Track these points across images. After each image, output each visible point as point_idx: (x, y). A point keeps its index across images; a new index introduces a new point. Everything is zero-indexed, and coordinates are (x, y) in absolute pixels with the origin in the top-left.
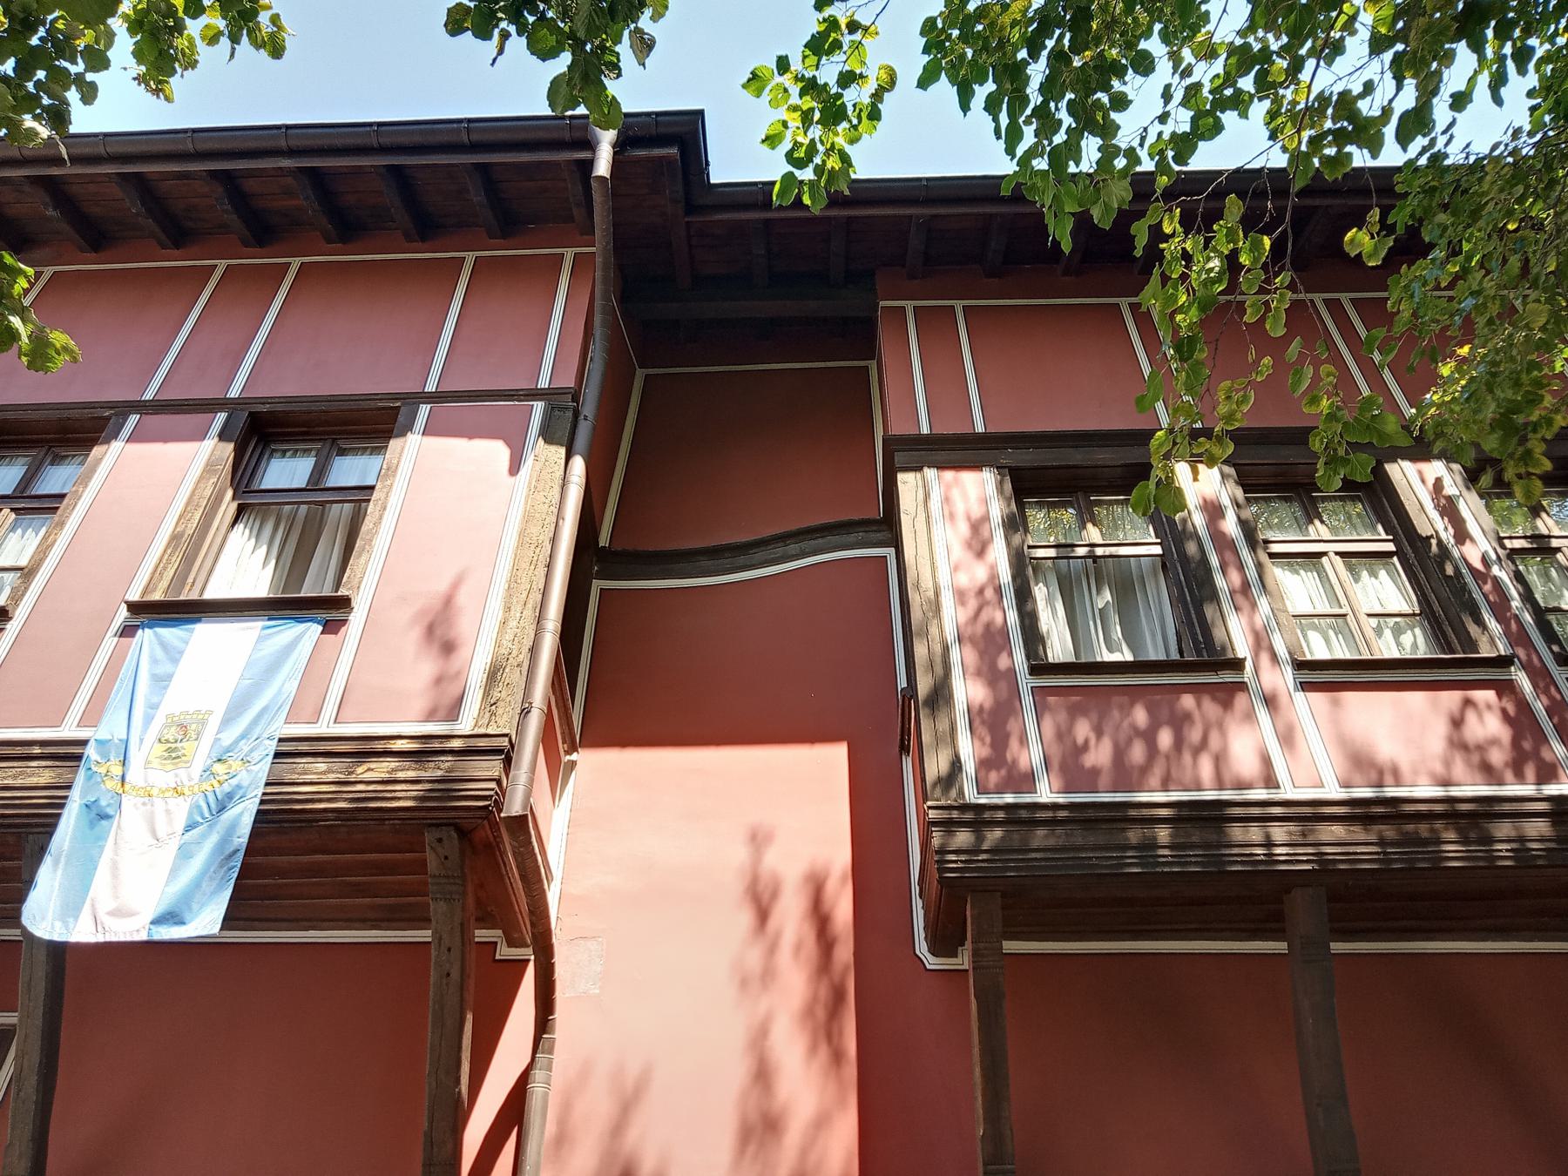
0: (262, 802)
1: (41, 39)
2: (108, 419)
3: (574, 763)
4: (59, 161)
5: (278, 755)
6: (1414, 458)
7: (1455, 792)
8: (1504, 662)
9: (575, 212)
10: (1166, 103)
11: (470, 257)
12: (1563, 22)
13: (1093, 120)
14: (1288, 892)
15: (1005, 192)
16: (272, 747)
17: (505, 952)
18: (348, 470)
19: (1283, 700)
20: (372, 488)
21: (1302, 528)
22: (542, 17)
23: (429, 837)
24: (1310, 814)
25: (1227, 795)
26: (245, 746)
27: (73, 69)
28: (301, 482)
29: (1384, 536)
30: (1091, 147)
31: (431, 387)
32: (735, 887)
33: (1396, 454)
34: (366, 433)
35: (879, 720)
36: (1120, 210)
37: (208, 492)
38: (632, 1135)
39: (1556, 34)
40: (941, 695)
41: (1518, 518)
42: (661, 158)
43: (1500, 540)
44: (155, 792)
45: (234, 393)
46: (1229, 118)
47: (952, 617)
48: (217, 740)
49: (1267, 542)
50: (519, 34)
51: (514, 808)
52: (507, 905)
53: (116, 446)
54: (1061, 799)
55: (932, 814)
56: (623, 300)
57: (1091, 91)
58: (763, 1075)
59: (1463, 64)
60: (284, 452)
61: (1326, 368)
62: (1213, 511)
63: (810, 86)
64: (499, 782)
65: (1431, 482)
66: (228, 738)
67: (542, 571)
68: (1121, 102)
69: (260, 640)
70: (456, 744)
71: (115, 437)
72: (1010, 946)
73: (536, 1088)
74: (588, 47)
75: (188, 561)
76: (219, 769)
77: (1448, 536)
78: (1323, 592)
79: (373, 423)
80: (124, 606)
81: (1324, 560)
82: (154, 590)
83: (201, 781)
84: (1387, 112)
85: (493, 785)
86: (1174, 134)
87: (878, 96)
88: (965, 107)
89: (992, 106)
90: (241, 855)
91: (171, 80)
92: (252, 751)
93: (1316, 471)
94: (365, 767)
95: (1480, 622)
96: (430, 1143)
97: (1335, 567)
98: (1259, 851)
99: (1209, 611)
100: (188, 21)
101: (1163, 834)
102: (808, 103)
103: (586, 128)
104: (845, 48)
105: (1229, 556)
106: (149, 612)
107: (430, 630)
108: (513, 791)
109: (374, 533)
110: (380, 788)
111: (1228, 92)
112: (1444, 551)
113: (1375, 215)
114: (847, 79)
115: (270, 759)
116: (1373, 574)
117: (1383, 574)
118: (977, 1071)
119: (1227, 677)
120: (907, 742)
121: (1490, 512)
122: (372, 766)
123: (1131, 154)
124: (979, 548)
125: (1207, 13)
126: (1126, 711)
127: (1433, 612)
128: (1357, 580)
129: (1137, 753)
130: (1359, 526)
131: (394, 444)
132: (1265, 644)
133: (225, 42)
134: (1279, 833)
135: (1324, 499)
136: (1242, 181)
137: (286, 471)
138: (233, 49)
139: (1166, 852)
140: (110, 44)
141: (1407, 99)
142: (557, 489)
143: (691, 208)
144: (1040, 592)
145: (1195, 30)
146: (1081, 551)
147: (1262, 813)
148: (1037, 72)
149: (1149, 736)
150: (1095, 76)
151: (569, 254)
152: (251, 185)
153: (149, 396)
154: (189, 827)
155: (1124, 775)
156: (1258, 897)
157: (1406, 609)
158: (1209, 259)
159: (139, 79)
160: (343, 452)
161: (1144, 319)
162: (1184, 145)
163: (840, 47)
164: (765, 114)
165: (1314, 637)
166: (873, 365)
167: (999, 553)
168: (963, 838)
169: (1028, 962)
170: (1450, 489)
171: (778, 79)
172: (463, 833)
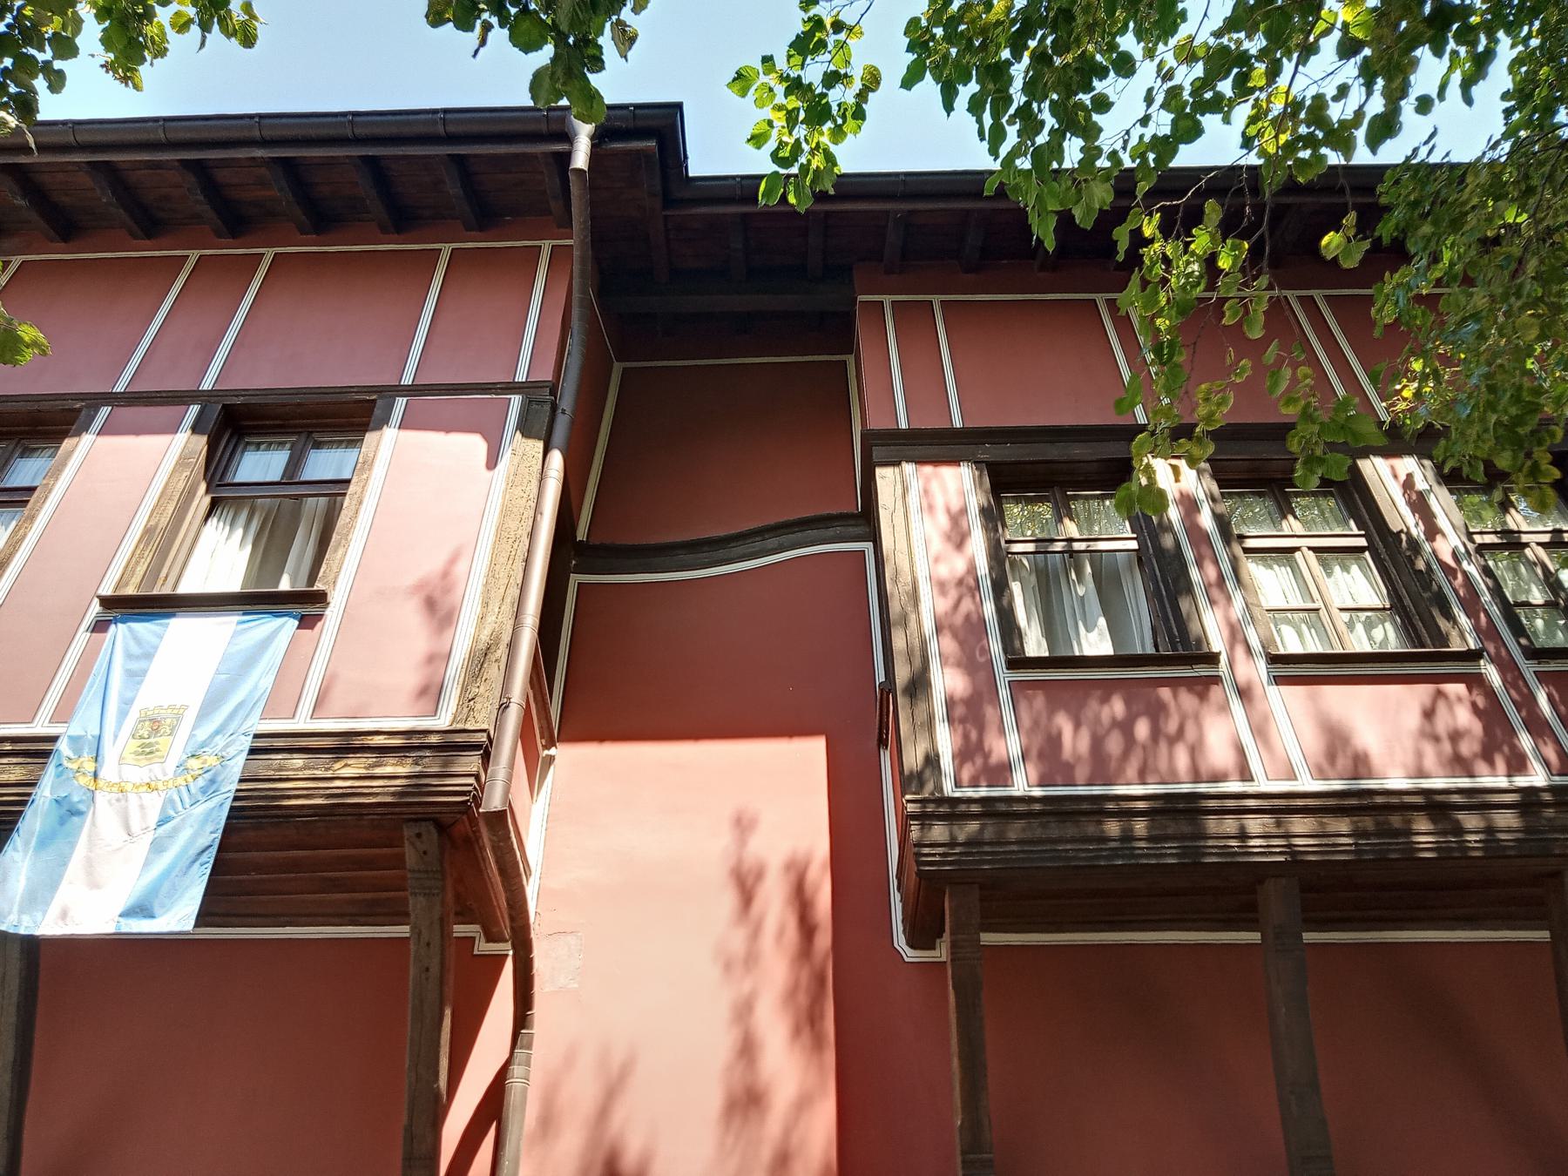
0: (236, 799)
1: (8, 26)
2: (79, 410)
3: (551, 759)
4: (26, 149)
5: (253, 751)
6: (1387, 453)
8: (1473, 656)
9: (553, 204)
10: (1149, 106)
11: (446, 249)
12: (1537, 24)
13: (1076, 122)
14: (1261, 882)
15: (989, 189)
16: (247, 743)
17: (483, 947)
18: (323, 463)
19: (1258, 691)
20: (348, 482)
21: (1275, 524)
22: (525, 10)
23: (408, 832)
24: (1282, 806)
25: (1203, 788)
26: (220, 741)
27: (41, 57)
28: (275, 475)
29: (1356, 532)
30: (1073, 150)
31: (407, 380)
33: (1366, 453)
34: (335, 426)
35: (859, 715)
36: (1101, 210)
37: (181, 485)
39: (1529, 36)
40: (919, 685)
41: (1488, 514)
42: (638, 151)
43: (1470, 535)
44: (129, 787)
45: (207, 385)
46: (1210, 121)
47: (931, 606)
48: (191, 736)
49: (1242, 537)
50: (502, 26)
51: (493, 802)
52: (485, 898)
53: (87, 439)
54: (1037, 792)
55: (911, 808)
56: (602, 292)
57: (1071, 88)
58: (747, 1049)
59: (1429, 70)
60: (270, 444)
61: (1304, 370)
62: (1190, 505)
63: (795, 86)
64: (477, 777)
65: (1403, 478)
66: (203, 734)
67: (519, 566)
68: (1103, 104)
69: (236, 634)
70: (434, 739)
71: (86, 429)
72: (988, 938)
73: (515, 1083)
74: (571, 40)
75: (162, 553)
76: (194, 764)
77: (1418, 532)
78: (1296, 587)
79: (349, 416)
80: (96, 601)
81: (1298, 555)
82: (127, 584)
83: (176, 775)
84: (1359, 113)
85: (471, 780)
86: (1154, 136)
87: (862, 96)
88: (949, 107)
89: (975, 107)
90: (214, 850)
91: (140, 68)
92: (227, 746)
93: (1293, 471)
94: (342, 763)
95: (1450, 617)
96: (410, 1137)
97: (1308, 562)
98: (1233, 843)
99: (1185, 604)
100: (158, 9)
101: (1140, 827)
102: (793, 102)
103: (563, 120)
104: (830, 47)
105: (1205, 550)
106: (121, 607)
108: (492, 788)
109: (350, 527)
110: (357, 783)
111: (1209, 95)
112: (1415, 546)
113: (1350, 219)
114: (832, 79)
115: (244, 755)
116: (1345, 569)
117: (1355, 568)
118: (955, 1062)
119: (1202, 671)
120: (885, 735)
121: (1461, 508)
122: (350, 762)
123: (1113, 155)
124: (958, 539)
125: (1184, 12)
126: (1105, 700)
127: (1404, 607)
128: (1329, 575)
129: (1114, 744)
130: (1331, 520)
131: (370, 437)
132: (1240, 637)
133: (195, 30)
134: (1254, 824)
135: (1297, 495)
136: (1224, 182)
137: (260, 464)
138: (204, 37)
139: (1142, 844)
140: (77, 29)
141: (1376, 105)
142: (535, 483)
143: (668, 201)
144: (1016, 587)
145: (1173, 30)
146: (1059, 546)
147: (1237, 806)
148: (1019, 71)
149: (1126, 727)
150: (1076, 78)
151: (546, 245)
152: (222, 175)
153: (120, 387)
154: (160, 823)
156: (1230, 889)
157: (1377, 603)
158: (1188, 263)
159: (107, 67)
160: (318, 445)
161: (1124, 324)
162: (1165, 146)
163: (825, 46)
164: (750, 113)
165: (1287, 630)
166: (851, 359)
167: (977, 544)
168: (939, 832)
169: (1007, 958)
170: (1421, 485)
171: (763, 79)
172: (442, 828)
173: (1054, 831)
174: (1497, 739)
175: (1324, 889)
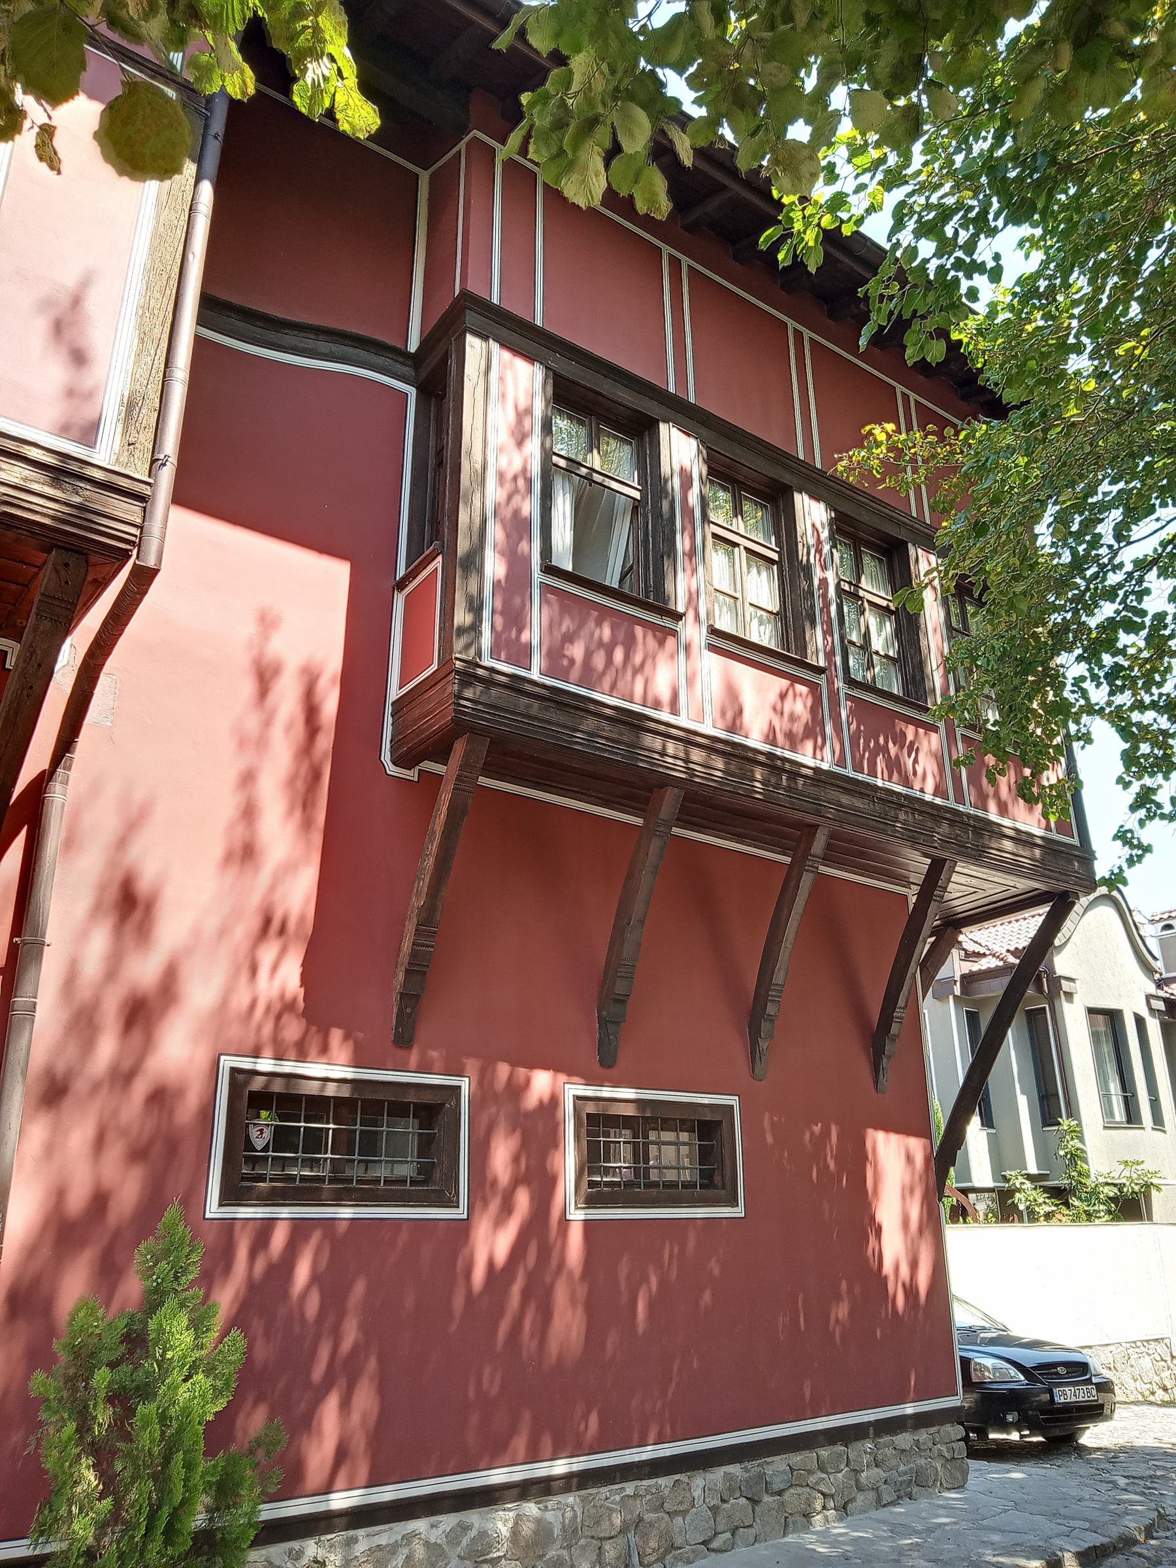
7: (778, 752)
8: (820, 671)
19: (695, 650)
24: (689, 739)
32: (243, 660)
38: (135, 852)
47: (494, 493)
72: (483, 781)
81: (736, 549)
97: (740, 554)
105: (689, 527)
107: (58, 328)
117: (764, 574)
119: (667, 622)
124: (520, 439)
129: (599, 661)
134: (671, 748)
146: (584, 471)
147: (665, 732)
155: (589, 677)
156: (635, 785)
167: (533, 446)
173: (553, 715)
174: (813, 730)
175: (705, 806)
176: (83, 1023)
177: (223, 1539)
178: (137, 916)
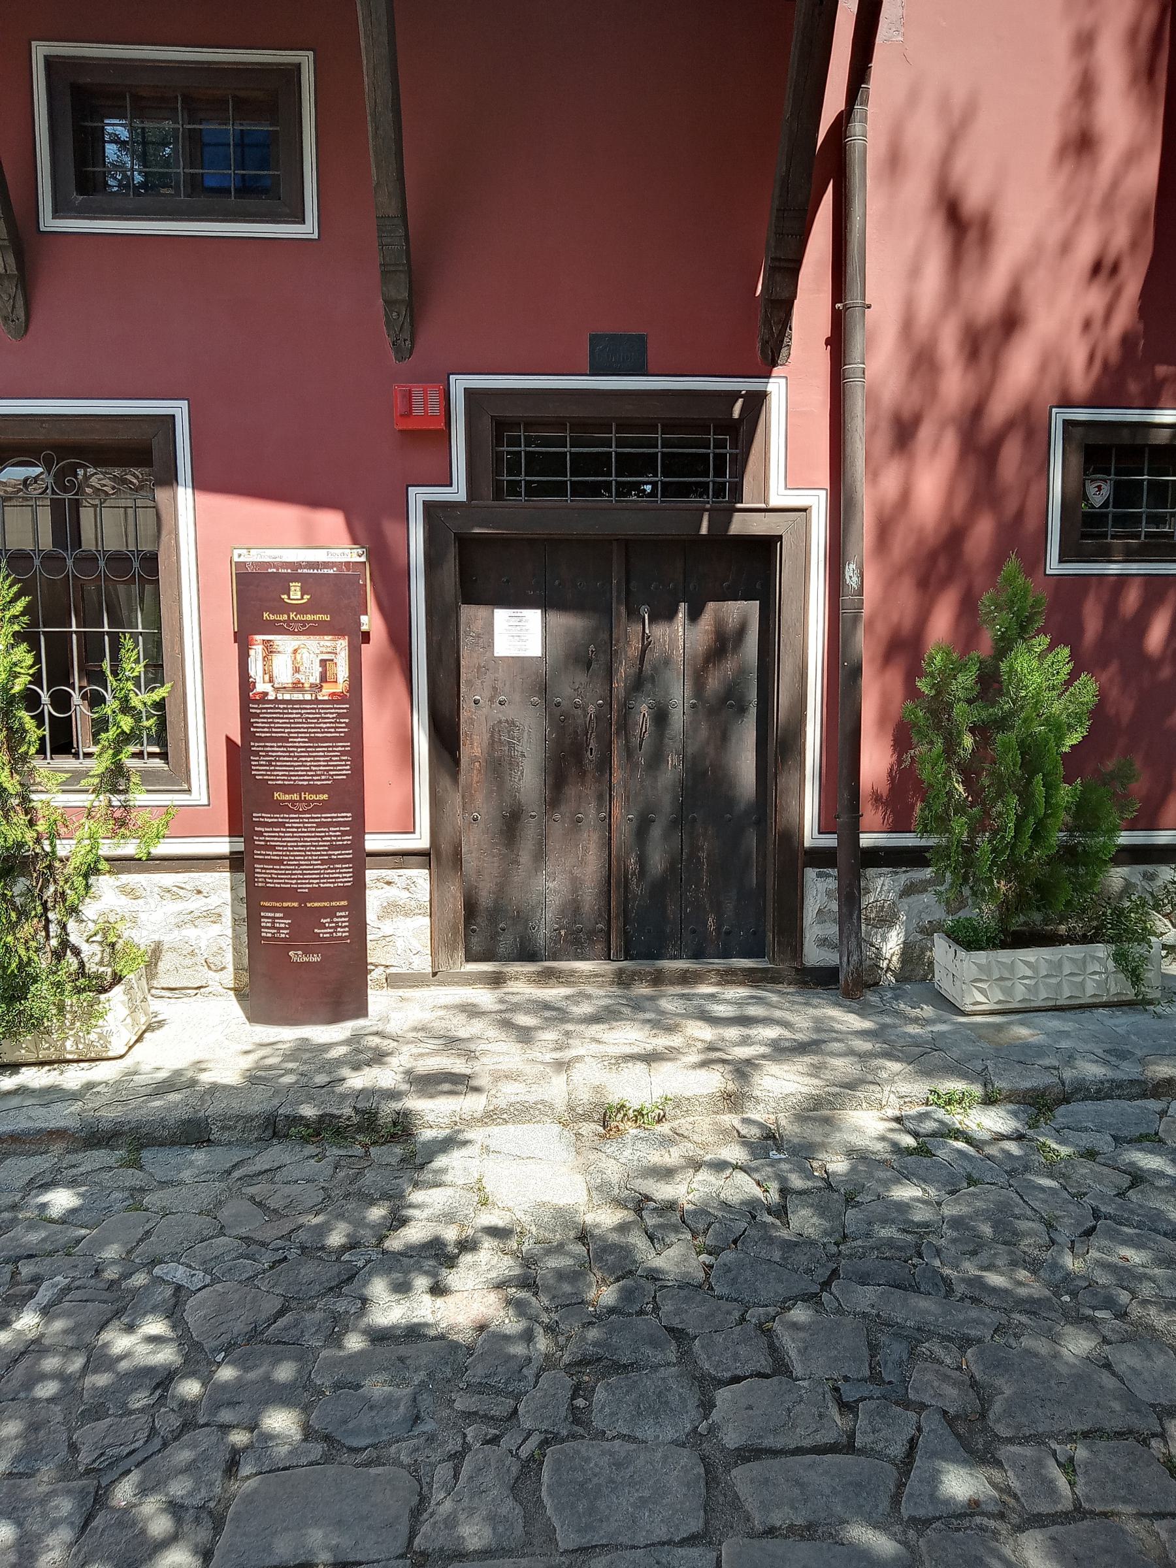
176: (922, 363)
177: (1084, 851)
178: (972, 235)
